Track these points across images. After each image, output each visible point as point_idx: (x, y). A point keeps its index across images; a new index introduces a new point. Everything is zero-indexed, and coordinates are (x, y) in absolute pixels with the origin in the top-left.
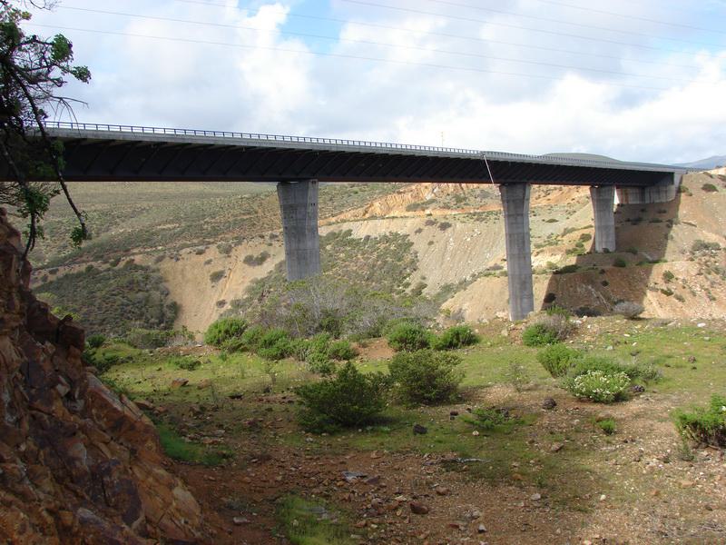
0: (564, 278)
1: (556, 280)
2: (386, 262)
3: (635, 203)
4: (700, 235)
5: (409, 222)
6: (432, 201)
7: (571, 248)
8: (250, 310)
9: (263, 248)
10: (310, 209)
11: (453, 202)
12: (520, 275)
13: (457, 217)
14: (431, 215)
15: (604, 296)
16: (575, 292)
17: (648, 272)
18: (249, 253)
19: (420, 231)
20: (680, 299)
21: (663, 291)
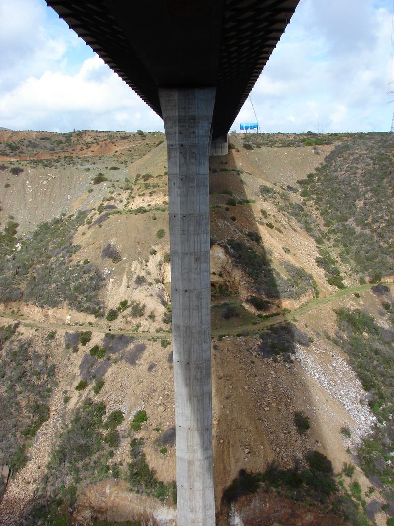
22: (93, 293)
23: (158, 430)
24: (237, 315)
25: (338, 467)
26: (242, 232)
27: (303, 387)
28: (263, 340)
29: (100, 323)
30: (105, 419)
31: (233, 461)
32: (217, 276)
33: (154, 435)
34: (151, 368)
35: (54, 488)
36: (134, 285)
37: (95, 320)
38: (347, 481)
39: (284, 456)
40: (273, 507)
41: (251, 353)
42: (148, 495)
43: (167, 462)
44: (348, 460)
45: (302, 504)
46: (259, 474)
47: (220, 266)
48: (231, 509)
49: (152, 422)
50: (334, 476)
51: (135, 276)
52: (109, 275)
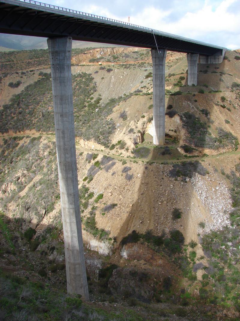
0: (176, 97)
1: (172, 99)
2: (80, 87)
3: (203, 63)
4: (234, 80)
5: (91, 68)
6: (101, 58)
7: (176, 83)
8: (13, 110)
9: (18, 79)
10: (67, 54)
11: (112, 59)
12: (160, 95)
13: (115, 66)
14: (101, 65)
15: (196, 107)
16: (182, 104)
17: (214, 96)
18: (11, 81)
19: (97, 72)
20: (229, 110)
21: (221, 106)
22: (107, 135)
23: (105, 204)
24: (170, 154)
25: (188, 241)
26: (198, 108)
27: (188, 197)
28: (174, 168)
29: (106, 151)
30: (86, 195)
31: (133, 225)
32: (174, 132)
33: (103, 206)
34: (113, 174)
35: (56, 222)
36: (127, 133)
37: (104, 149)
38: (190, 249)
39: (159, 229)
40: (144, 252)
41: (164, 174)
42: (90, 233)
43: (103, 219)
44: (195, 239)
45: (158, 254)
46: (142, 234)
47: (176, 127)
48: (123, 248)
49: (104, 200)
50: (183, 245)
51: (130, 128)
52: (119, 127)
